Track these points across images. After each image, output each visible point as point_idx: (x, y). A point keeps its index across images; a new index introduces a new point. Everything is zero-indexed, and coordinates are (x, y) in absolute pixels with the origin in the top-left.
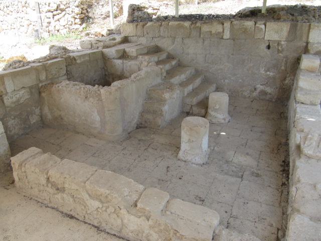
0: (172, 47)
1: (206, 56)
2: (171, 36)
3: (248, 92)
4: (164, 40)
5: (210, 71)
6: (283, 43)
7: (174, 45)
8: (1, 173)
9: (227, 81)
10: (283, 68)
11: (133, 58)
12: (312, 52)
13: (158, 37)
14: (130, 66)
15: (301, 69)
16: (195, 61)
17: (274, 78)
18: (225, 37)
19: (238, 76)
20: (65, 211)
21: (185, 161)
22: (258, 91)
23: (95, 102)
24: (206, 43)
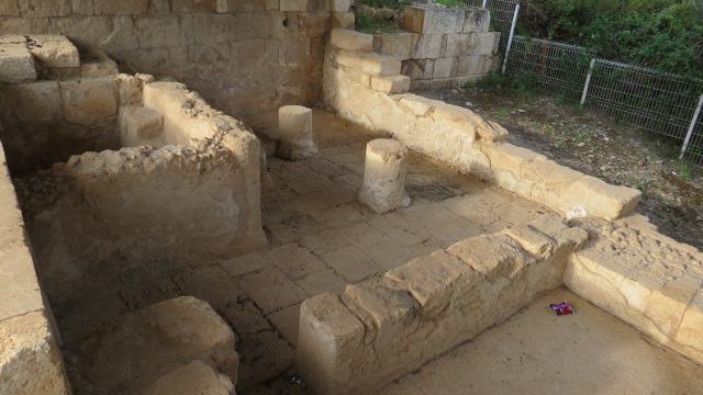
0: (109, 39)
1: (188, 49)
2: (102, 14)
3: (267, 101)
4: (87, 21)
5: (202, 77)
6: (304, 15)
7: (114, 33)
8: (596, 2)
9: (232, 90)
10: (308, 53)
11: (69, 72)
12: (344, 26)
13: (67, 16)
14: (87, 93)
15: (331, 46)
16: (167, 64)
17: (299, 70)
18: (219, 10)
19: (249, 77)
20: (547, 233)
21: (281, 375)
22: (281, 95)
23: (226, 175)
24: (185, 23)
